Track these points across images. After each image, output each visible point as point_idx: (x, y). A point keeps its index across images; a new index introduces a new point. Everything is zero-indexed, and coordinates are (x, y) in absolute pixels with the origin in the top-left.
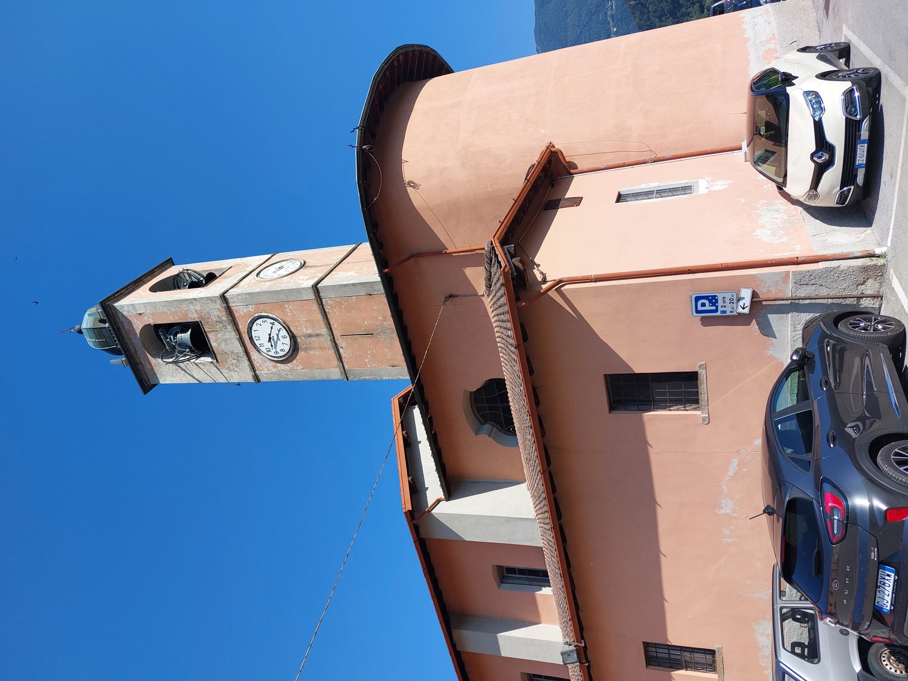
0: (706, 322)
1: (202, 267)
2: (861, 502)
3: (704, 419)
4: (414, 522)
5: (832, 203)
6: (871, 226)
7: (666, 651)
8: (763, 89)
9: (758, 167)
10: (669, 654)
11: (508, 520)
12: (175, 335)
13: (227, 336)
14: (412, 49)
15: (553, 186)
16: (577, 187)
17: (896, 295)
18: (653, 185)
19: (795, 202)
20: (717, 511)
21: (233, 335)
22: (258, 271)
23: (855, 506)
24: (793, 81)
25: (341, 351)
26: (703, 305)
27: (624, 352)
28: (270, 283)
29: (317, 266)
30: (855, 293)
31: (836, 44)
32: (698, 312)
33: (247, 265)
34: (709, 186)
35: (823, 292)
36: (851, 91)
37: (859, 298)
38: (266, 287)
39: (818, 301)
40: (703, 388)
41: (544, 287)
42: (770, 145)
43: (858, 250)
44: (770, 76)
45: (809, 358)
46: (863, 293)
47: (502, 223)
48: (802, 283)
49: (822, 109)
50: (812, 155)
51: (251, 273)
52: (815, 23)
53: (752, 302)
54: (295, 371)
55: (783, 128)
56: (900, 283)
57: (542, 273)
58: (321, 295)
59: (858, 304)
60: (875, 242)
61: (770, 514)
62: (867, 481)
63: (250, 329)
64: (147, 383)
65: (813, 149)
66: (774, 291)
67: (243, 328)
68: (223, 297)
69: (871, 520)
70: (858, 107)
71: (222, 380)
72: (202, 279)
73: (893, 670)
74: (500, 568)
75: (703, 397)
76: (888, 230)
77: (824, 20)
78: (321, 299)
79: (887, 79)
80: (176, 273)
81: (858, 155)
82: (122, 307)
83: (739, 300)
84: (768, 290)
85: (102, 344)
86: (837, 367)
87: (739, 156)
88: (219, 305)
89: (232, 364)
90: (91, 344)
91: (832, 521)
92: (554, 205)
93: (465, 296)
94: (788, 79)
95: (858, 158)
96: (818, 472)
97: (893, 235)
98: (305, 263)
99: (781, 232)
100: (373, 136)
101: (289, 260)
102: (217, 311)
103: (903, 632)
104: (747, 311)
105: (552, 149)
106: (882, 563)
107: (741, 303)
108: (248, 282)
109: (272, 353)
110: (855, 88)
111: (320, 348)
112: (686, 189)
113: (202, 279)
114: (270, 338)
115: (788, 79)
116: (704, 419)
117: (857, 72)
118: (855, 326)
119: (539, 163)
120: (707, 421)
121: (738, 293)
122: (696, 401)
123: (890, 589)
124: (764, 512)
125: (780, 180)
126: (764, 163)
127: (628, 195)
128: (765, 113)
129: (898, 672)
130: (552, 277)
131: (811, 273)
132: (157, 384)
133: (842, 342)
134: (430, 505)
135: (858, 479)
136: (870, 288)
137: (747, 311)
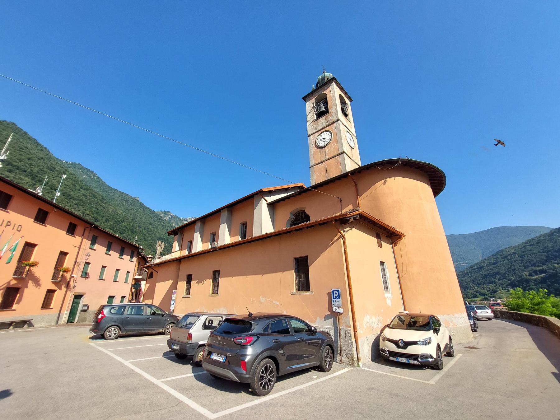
0: (329, 294)
1: (350, 112)
2: (250, 352)
3: (292, 292)
4: (259, 193)
5: (381, 346)
6: (372, 361)
7: (218, 278)
8: (432, 321)
9: (396, 317)
10: (217, 278)
11: (261, 225)
12: (324, 105)
13: (324, 123)
14: (444, 179)
15: (386, 237)
16: (386, 246)
17: (341, 369)
18: (388, 276)
19: (382, 331)
20: (261, 296)
21: (324, 125)
22: (349, 132)
23: (248, 349)
24: (436, 333)
25: (320, 164)
26: (336, 294)
27: (316, 263)
28: (345, 136)
29: (352, 153)
30: (342, 353)
31: (453, 351)
32: (333, 291)
33: (351, 128)
34: (388, 298)
35: (343, 341)
36: (432, 357)
37: (340, 354)
38: (343, 135)
39: (339, 338)
40: (304, 293)
41: (342, 231)
42: (407, 322)
43: (361, 355)
44: (437, 323)
45: (313, 334)
46: (342, 356)
47: (369, 215)
48: (346, 332)
49: (423, 345)
50: (402, 340)
51: (348, 129)
52: (462, 342)
53: (338, 313)
54: (312, 149)
55: (414, 328)
56: (346, 372)
57: (348, 231)
58: (341, 155)
59: (338, 354)
60: (365, 363)
61: (249, 315)
62: (257, 355)
63: (327, 131)
64: (306, 98)
65: (405, 340)
66: (342, 321)
67: (327, 129)
68: (338, 120)
69: (243, 354)
70: (424, 360)
71: (308, 124)
72: (345, 112)
73: (200, 355)
74: (246, 223)
75: (300, 292)
76: (369, 368)
77: (463, 346)
78: (339, 155)
79: (438, 373)
80: (347, 103)
81: (402, 358)
82: (333, 85)
83: (338, 307)
84: (343, 319)
85: (319, 81)
86: (314, 344)
87: (402, 310)
88: (335, 119)
89: (314, 127)
90: (319, 77)
91: (241, 339)
92: (378, 236)
93: (341, 206)
94: (436, 331)
95: (401, 358)
96: (262, 335)
97: (367, 370)
98: (353, 148)
99: (368, 325)
100: (405, 165)
101: (354, 143)
102: (333, 118)
103: (206, 362)
104: (334, 310)
105: (402, 236)
106: (227, 357)
107: (337, 308)
108: (345, 128)
109: (318, 140)
110: (433, 359)
111: (321, 157)
112: (386, 288)
113: (345, 112)
114: (324, 139)
115: (436, 331)
116: (292, 292)
117: (441, 360)
118: (328, 353)
119: (396, 230)
120: (292, 293)
121: (341, 307)
122: (299, 290)
123: (218, 359)
124: (250, 313)
125: (391, 326)
126: (399, 319)
127: (383, 266)
128: (421, 321)
129: (199, 357)
130: (346, 234)
131: (350, 336)
132: (305, 101)
133: (321, 347)
134: (265, 198)
135: (259, 351)
136: (345, 359)
137: (334, 310)
